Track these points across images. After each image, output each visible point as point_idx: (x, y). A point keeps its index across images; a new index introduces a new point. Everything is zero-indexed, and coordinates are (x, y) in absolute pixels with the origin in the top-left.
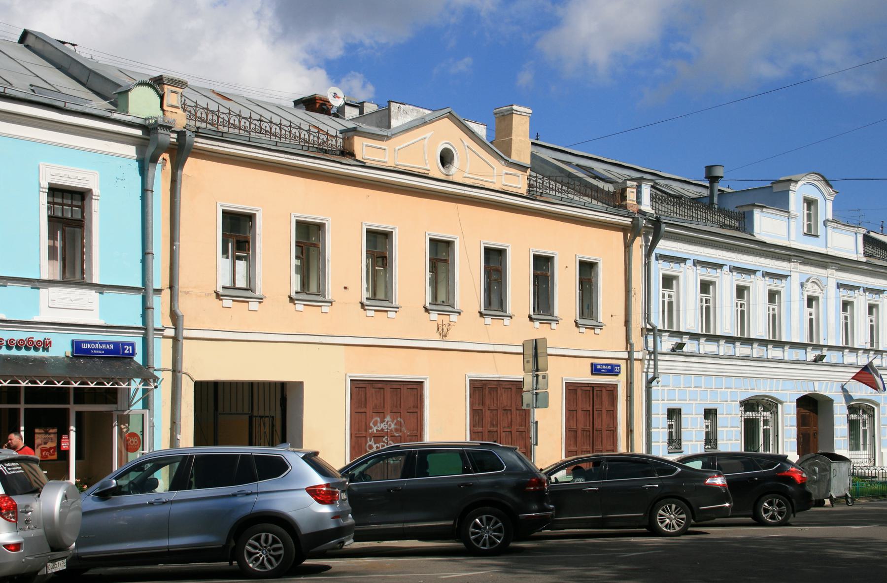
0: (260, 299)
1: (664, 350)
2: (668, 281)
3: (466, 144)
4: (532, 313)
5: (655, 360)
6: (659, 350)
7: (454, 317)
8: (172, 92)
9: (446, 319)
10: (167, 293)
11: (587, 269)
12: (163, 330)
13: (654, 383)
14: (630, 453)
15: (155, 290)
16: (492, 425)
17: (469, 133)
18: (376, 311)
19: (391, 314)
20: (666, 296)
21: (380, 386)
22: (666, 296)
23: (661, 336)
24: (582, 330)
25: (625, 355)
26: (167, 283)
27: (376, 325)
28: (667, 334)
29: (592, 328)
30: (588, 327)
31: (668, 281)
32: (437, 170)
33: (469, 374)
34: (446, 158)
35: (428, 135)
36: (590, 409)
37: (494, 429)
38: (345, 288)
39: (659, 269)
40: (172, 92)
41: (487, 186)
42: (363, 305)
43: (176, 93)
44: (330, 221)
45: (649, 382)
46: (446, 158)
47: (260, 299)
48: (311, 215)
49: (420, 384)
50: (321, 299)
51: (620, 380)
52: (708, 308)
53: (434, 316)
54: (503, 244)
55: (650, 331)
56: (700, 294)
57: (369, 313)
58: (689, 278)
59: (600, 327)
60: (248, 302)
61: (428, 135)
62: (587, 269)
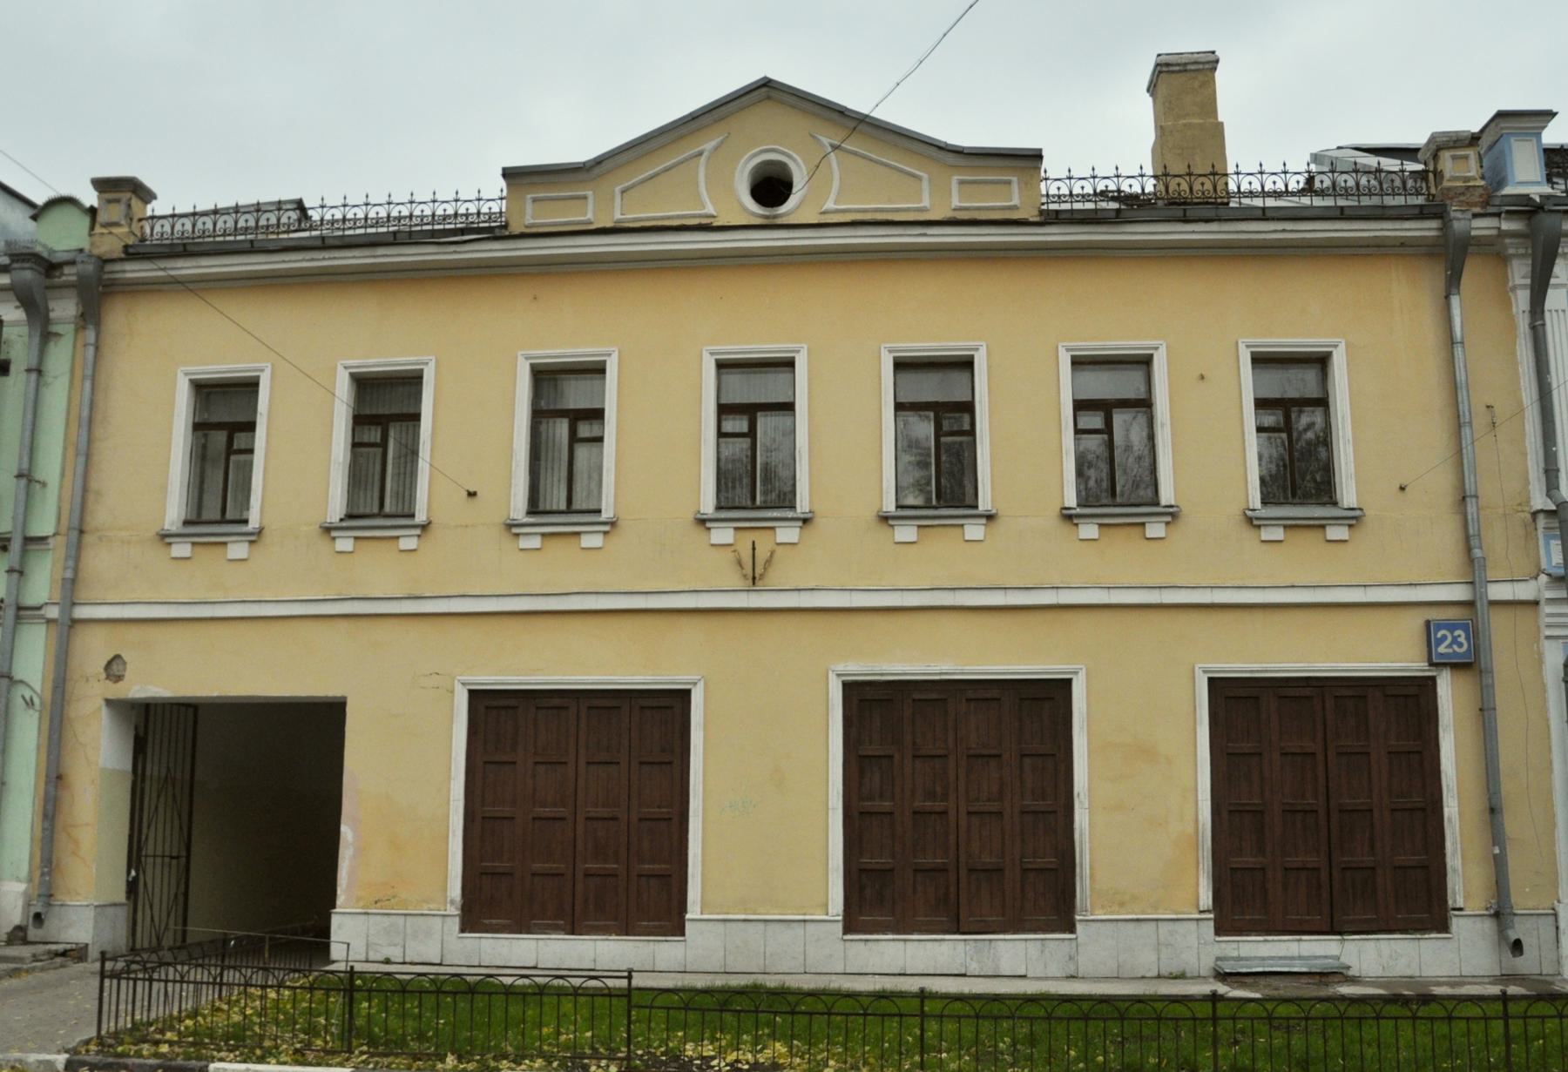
0: (1354, 519)
7: (787, 534)
9: (764, 543)
10: (58, 546)
16: (931, 795)
18: (543, 535)
19: (591, 541)
21: (556, 702)
25: (1460, 593)
30: (1291, 526)
33: (840, 668)
34: (771, 187)
46: (771, 187)
47: (256, 537)
53: (723, 534)
57: (524, 543)
60: (225, 544)
61: (708, 146)
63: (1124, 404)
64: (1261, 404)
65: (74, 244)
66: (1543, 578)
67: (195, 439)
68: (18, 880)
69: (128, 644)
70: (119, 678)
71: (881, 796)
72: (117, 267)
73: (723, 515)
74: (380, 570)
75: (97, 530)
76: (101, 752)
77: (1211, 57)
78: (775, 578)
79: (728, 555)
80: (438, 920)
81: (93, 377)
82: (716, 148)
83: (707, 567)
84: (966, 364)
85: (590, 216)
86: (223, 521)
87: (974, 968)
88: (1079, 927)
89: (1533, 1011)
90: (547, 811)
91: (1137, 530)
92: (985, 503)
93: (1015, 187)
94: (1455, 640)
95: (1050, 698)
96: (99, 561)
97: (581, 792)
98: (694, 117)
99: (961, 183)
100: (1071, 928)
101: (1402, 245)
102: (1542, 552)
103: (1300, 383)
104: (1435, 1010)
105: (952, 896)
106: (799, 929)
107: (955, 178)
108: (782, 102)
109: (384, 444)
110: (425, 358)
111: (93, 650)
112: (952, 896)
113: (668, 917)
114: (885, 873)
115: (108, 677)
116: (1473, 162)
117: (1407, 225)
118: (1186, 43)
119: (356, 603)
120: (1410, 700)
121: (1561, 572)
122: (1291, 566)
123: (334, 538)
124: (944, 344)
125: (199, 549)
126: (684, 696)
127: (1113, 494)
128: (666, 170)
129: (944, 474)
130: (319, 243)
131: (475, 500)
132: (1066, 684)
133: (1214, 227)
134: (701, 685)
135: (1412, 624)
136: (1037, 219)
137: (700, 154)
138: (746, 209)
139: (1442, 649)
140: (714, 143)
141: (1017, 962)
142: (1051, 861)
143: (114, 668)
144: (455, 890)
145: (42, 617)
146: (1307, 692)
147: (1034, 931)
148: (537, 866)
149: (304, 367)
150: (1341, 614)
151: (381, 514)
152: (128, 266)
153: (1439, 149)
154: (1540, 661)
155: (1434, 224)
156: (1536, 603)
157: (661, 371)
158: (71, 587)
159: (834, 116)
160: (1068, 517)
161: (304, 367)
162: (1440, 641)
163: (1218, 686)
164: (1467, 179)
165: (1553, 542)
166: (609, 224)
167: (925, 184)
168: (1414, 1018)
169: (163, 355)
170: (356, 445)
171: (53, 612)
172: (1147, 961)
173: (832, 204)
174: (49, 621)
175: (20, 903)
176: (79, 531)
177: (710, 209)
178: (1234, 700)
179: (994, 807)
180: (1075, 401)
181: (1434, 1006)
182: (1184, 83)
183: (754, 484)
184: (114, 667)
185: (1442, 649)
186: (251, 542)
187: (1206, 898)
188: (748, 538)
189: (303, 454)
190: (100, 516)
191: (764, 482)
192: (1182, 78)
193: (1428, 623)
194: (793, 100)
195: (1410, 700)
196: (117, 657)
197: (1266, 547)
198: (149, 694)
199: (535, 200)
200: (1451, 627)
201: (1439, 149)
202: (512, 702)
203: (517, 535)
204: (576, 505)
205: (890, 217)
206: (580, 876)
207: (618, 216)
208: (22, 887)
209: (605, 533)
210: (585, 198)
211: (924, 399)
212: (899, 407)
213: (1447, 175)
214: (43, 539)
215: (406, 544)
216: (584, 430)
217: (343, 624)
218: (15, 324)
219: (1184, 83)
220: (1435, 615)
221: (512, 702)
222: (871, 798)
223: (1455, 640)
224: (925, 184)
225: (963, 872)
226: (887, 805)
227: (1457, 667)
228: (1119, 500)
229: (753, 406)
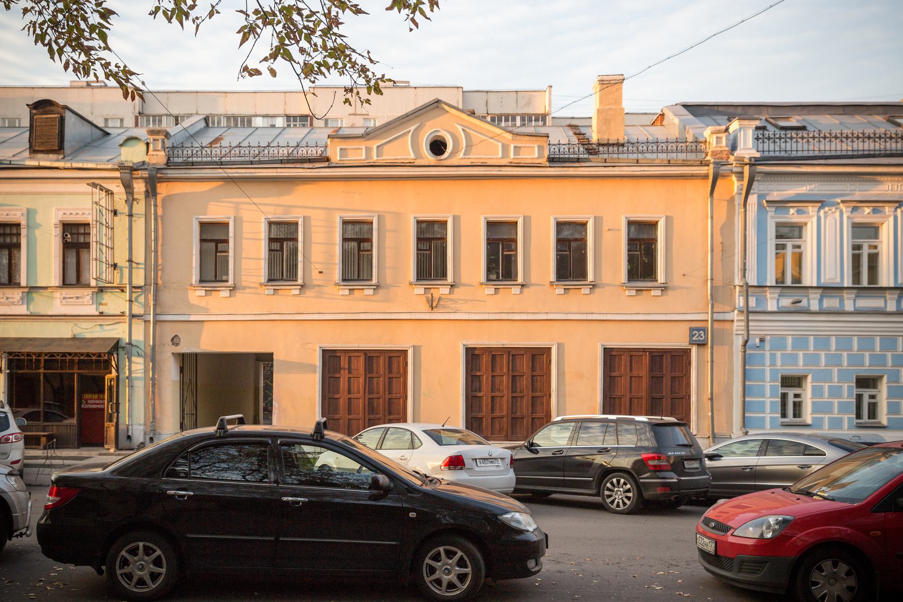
7: (445, 290)
27: (361, 302)
33: (465, 343)
34: (438, 147)
35: (413, 128)
41: (490, 162)
46: (438, 147)
47: (664, 288)
49: (473, 355)
61: (413, 128)
65: (141, 160)
66: (736, 312)
67: (270, 255)
68: (140, 425)
70: (177, 345)
72: (164, 171)
74: (288, 299)
76: (171, 374)
77: (621, 77)
86: (216, 281)
94: (700, 335)
98: (407, 116)
109: (282, 249)
117: (695, 168)
118: (610, 70)
120: (680, 358)
133: (686, 168)
135: (685, 328)
139: (694, 338)
143: (175, 341)
150: (650, 321)
151: (282, 279)
152: (169, 171)
161: (250, 220)
162: (693, 336)
165: (741, 298)
170: (270, 250)
175: (142, 433)
182: (610, 85)
185: (694, 338)
189: (250, 254)
195: (680, 358)
208: (142, 427)
218: (118, 193)
219: (610, 85)
223: (700, 335)
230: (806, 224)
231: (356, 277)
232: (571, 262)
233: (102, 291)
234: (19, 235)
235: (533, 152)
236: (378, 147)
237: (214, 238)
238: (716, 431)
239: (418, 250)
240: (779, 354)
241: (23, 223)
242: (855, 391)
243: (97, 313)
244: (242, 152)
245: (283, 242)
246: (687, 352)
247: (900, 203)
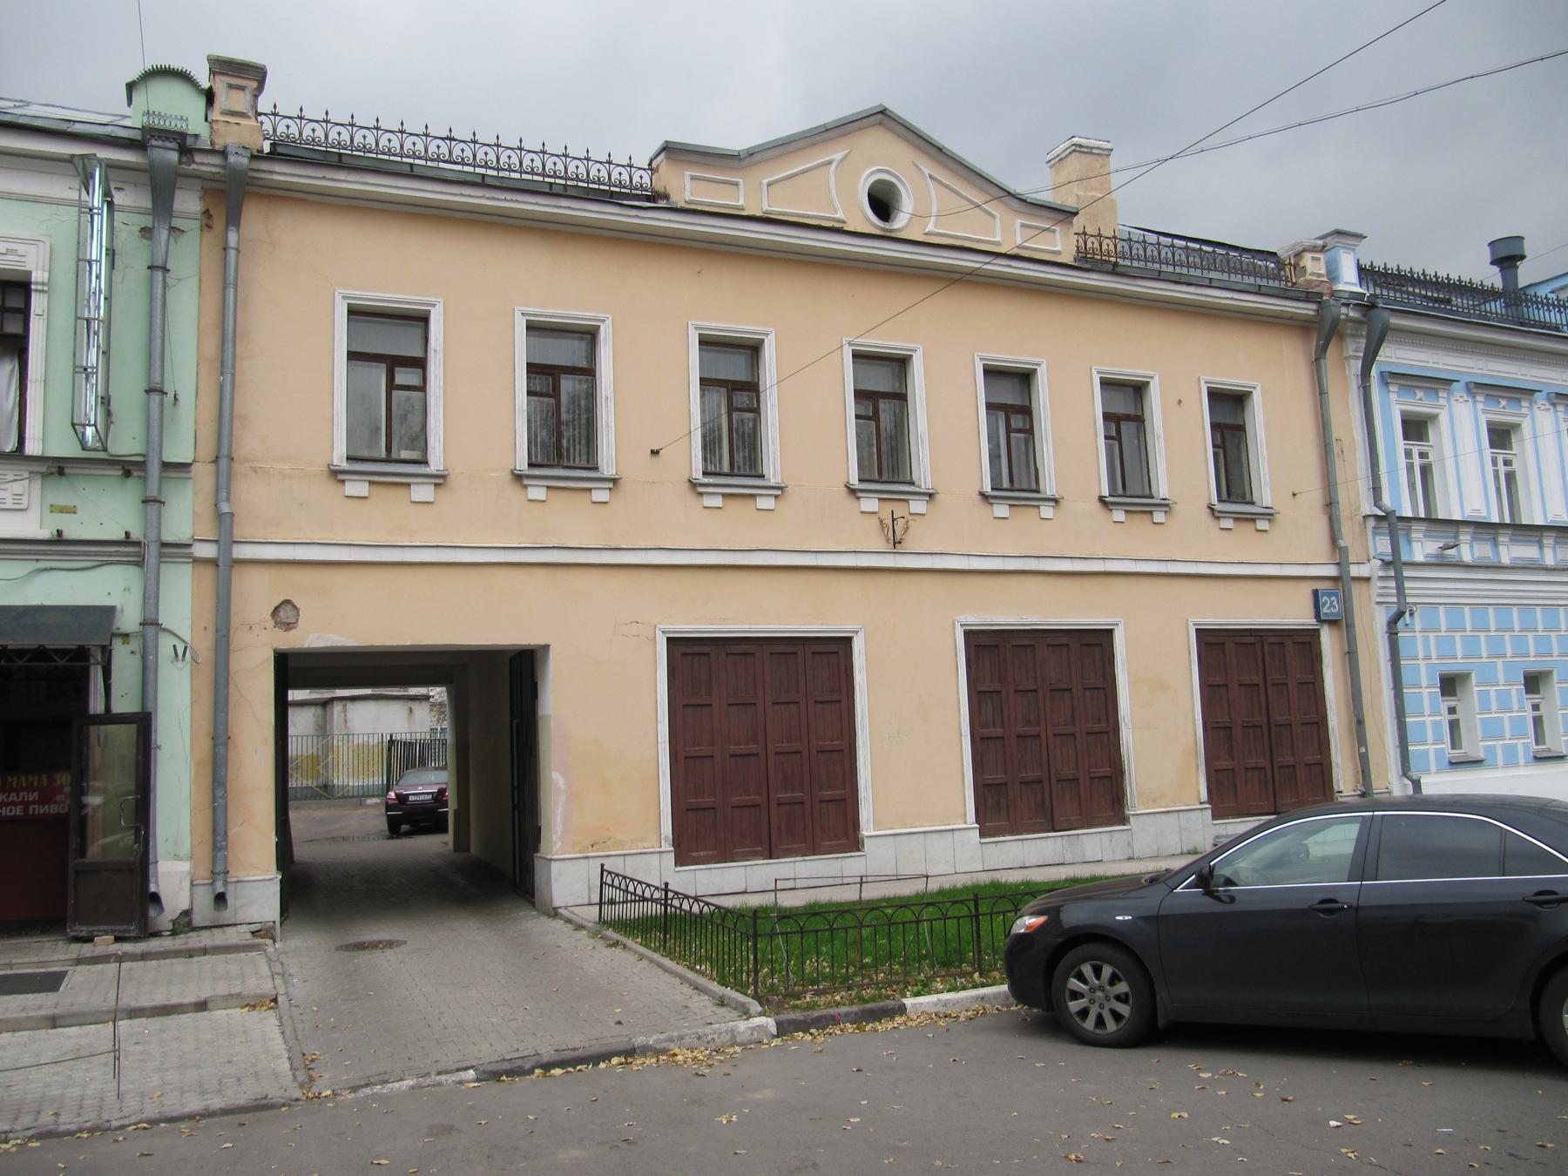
0: (780, 491)
1: (1419, 558)
2: (1415, 427)
3: (926, 172)
4: (1214, 500)
5: (1399, 580)
6: (1404, 558)
7: (918, 506)
8: (231, 86)
9: (900, 510)
10: (203, 474)
11: (1229, 407)
12: (189, 546)
13: (1400, 624)
14: (291, 794)
15: (167, 466)
16: (1028, 722)
17: (951, 164)
18: (724, 495)
19: (765, 503)
20: (1500, 462)
22: (1500, 462)
23: (1409, 531)
24: (1228, 523)
25: (1331, 571)
26: (207, 451)
27: (1011, 536)
28: (1423, 527)
29: (1251, 519)
30: (1240, 518)
31: (1415, 427)
32: (866, 219)
34: (882, 203)
35: (838, 156)
36: (1259, 680)
37: (1032, 730)
38: (655, 453)
39: (1391, 406)
40: (231, 86)
42: (693, 485)
43: (242, 88)
44: (1044, 366)
45: (1393, 622)
46: (882, 203)
48: (1011, 356)
49: (843, 645)
50: (911, 489)
51: (182, 600)
52: (1510, 477)
53: (870, 504)
54: (1028, 359)
55: (1388, 521)
56: (1488, 452)
57: (707, 502)
58: (1461, 425)
59: (1269, 516)
60: (409, 485)
61: (838, 156)
62: (1229, 407)
63: (1128, 418)
64: (532, 369)
69: (297, 586)
70: (288, 626)
71: (994, 725)
73: (537, 472)
74: (566, 520)
75: (247, 460)
78: (908, 545)
79: (875, 520)
80: (656, 857)
81: (227, 287)
82: (842, 160)
83: (855, 531)
84: (421, 319)
85: (741, 202)
87: (1069, 858)
88: (1132, 819)
89: (809, 926)
90: (742, 749)
91: (1146, 517)
92: (607, 467)
93: (1058, 235)
95: (1097, 643)
96: (252, 496)
97: (765, 733)
99: (1023, 226)
100: (1122, 819)
101: (1291, 318)
102: (1370, 543)
103: (563, 353)
104: (850, 920)
105: (1047, 804)
106: (949, 836)
107: (1019, 222)
108: (890, 130)
110: (602, 316)
111: (256, 595)
112: (1047, 804)
113: (847, 837)
114: (1001, 786)
115: (276, 624)
116: (1322, 263)
119: (556, 552)
120: (1305, 642)
121: (1390, 558)
122: (1233, 549)
123: (526, 487)
124: (1011, 357)
125: (378, 490)
126: (847, 642)
127: (560, 456)
128: (804, 172)
129: (734, 447)
130: (479, 180)
131: (655, 459)
132: (1109, 633)
133: (1191, 289)
134: (861, 634)
136: (1069, 260)
137: (830, 163)
138: (868, 220)
140: (842, 154)
141: (1091, 852)
142: (1105, 770)
143: (285, 614)
144: (667, 829)
145: (189, 556)
146: (1252, 640)
147: (1100, 825)
148: (736, 799)
149: (481, 310)
153: (1304, 250)
154: (1372, 619)
155: (1314, 307)
156: (1368, 579)
157: (809, 357)
158: (224, 521)
159: (932, 151)
160: (852, 492)
163: (970, 635)
164: (1320, 275)
166: (759, 214)
167: (998, 222)
168: (802, 932)
169: (312, 278)
171: (208, 551)
172: (1174, 843)
173: (931, 228)
174: (198, 561)
176: (223, 458)
177: (840, 215)
178: (692, 658)
179: (1070, 729)
180: (528, 364)
181: (849, 916)
183: (885, 457)
184: (282, 614)
185: (1325, 610)
186: (436, 485)
187: (1204, 795)
188: (889, 506)
190: (249, 442)
191: (378, 429)
192: (1091, 158)
193: (1315, 593)
194: (901, 129)
195: (1305, 642)
196: (287, 602)
197: (349, 501)
198: (329, 644)
199: (693, 178)
200: (1330, 595)
201: (1304, 250)
202: (705, 649)
203: (701, 494)
204: (394, 455)
205: (967, 244)
206: (773, 804)
207: (766, 208)
209: (776, 496)
210: (736, 184)
211: (722, 377)
212: (353, 356)
213: (1309, 270)
214: (184, 467)
215: (762, 503)
216: (404, 377)
217: (541, 572)
220: (1320, 586)
221: (705, 649)
222: (987, 726)
224: (998, 222)
225: (1054, 782)
226: (998, 731)
227: (1333, 623)
228: (885, 478)
229: (882, 393)
230: (1516, 427)
231: (726, 469)
232: (563, 430)
233: (61, 472)
234: (25, 312)
235: (1061, 244)
236: (769, 185)
237: (390, 347)
238: (301, 852)
239: (756, 411)
240: (1432, 635)
241: (38, 276)
242: (1444, 707)
243: (45, 534)
244: (504, 159)
245: (562, 383)
246: (1315, 633)
247: (1563, 399)
